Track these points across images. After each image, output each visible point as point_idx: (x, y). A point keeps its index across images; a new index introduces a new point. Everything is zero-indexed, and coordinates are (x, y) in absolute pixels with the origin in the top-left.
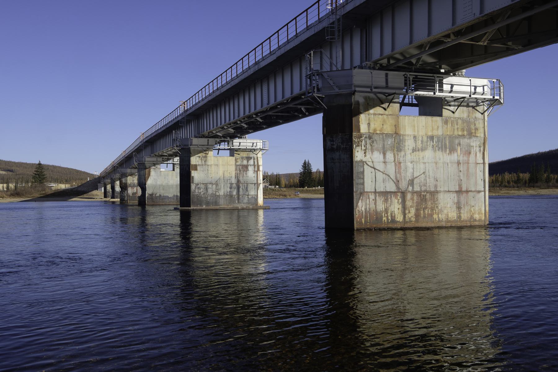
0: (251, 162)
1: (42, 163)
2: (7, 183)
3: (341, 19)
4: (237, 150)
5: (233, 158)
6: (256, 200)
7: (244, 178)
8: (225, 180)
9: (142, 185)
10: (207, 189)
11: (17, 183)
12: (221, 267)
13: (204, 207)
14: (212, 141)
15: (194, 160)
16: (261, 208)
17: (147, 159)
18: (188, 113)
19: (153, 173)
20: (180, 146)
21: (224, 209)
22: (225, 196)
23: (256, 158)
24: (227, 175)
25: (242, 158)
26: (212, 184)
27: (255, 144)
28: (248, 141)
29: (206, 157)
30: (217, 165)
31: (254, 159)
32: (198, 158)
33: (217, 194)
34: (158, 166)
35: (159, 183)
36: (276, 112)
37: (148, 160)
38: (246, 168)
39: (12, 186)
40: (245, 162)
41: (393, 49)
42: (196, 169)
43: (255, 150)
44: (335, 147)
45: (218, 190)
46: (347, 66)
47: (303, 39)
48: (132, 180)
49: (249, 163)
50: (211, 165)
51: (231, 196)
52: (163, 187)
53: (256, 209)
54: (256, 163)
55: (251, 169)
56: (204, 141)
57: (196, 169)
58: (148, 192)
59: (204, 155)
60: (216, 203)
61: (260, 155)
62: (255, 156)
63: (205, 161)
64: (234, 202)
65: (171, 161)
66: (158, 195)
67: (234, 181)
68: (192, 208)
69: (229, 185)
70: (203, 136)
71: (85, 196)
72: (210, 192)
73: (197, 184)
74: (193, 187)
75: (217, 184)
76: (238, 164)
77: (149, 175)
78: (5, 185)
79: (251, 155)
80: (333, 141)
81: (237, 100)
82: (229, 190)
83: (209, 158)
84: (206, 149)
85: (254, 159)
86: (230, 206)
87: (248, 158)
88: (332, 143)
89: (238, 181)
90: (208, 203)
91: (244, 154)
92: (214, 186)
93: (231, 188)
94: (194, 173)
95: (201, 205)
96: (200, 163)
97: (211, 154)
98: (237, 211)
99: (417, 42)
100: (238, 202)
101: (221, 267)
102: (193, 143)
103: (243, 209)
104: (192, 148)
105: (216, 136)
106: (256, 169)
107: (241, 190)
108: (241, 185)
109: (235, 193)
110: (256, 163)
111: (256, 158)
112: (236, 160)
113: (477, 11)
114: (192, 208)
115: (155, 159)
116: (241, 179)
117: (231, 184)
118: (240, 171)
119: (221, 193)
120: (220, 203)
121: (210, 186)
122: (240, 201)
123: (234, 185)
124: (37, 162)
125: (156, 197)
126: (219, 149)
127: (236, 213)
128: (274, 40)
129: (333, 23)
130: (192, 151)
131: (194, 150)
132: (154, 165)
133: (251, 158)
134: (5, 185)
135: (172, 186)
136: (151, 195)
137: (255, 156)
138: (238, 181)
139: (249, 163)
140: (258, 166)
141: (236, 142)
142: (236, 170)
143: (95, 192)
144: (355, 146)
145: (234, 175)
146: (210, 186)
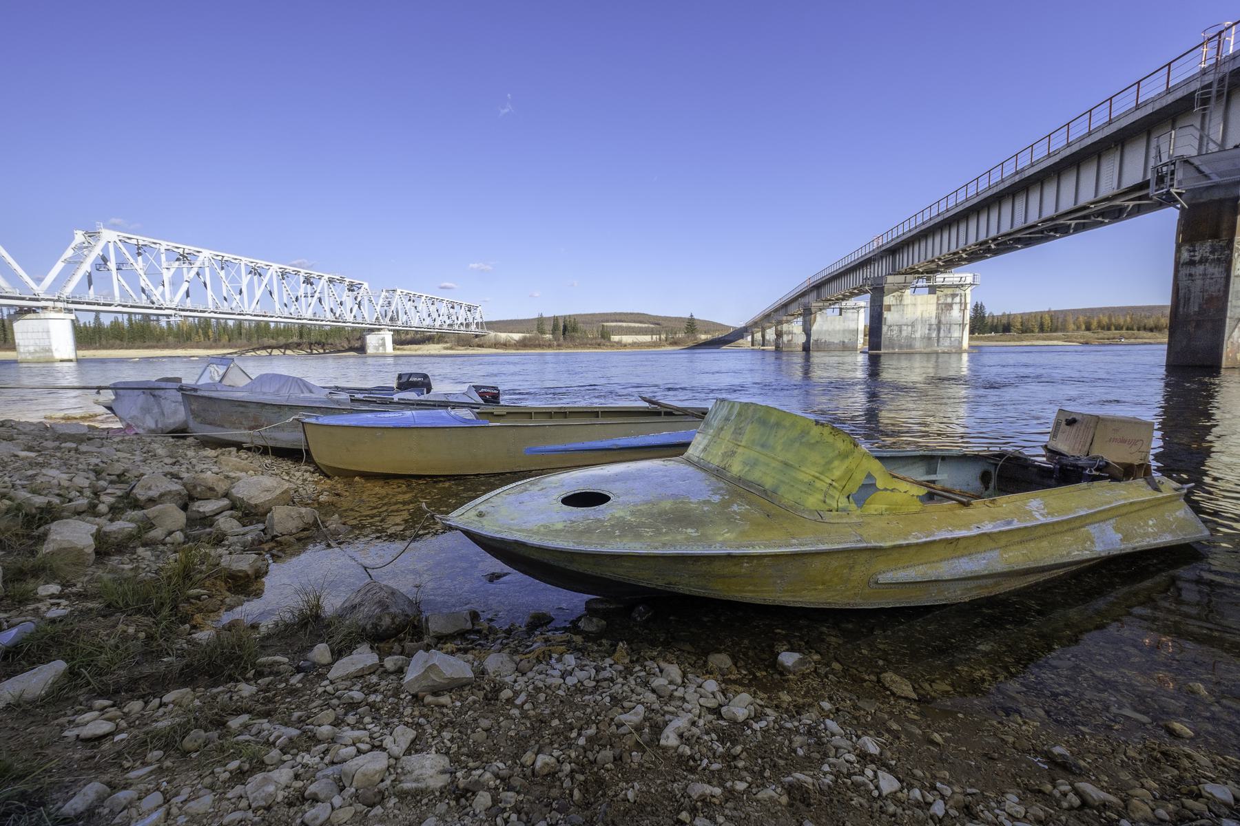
0: (957, 299)
1: (695, 317)
2: (660, 335)
3: (1227, 77)
4: (940, 287)
5: (935, 296)
6: (961, 342)
7: (947, 318)
8: (923, 321)
9: (807, 331)
10: (901, 331)
11: (667, 334)
12: (961, 441)
13: (897, 350)
14: (909, 277)
15: (888, 300)
16: (965, 351)
17: (813, 305)
18: (884, 248)
19: (819, 318)
20: (872, 285)
21: (921, 353)
22: (922, 338)
23: (963, 295)
24: (926, 315)
25: (946, 295)
26: (908, 325)
27: (963, 279)
28: (956, 275)
29: (902, 296)
30: (915, 305)
31: (961, 296)
32: (892, 299)
33: (913, 336)
34: (824, 311)
35: (825, 328)
36: (1030, 233)
37: (815, 305)
38: (949, 306)
39: (663, 337)
40: (949, 300)
41: (941, 253)
42: (890, 310)
43: (962, 285)
44: (1197, 258)
45: (914, 332)
46: (884, 274)
47: (1170, 102)
48: (796, 327)
49: (954, 301)
50: (907, 305)
51: (929, 339)
52: (829, 333)
53: (960, 352)
54: (963, 301)
55: (956, 308)
56: (900, 279)
57: (890, 310)
58: (813, 338)
59: (899, 294)
60: (910, 346)
61: (968, 292)
62: (963, 292)
63: (901, 301)
64: (932, 346)
65: (837, 306)
66: (823, 341)
67: (934, 321)
68: (882, 351)
69: (927, 326)
70: (899, 273)
71: (732, 344)
72: (904, 334)
73: (890, 326)
74: (885, 329)
75: (913, 325)
76: (940, 302)
77: (815, 320)
78: (658, 337)
79: (958, 291)
80: (1194, 251)
81: (939, 237)
82: (927, 331)
83: (905, 297)
84: (901, 288)
85: (961, 296)
86: (928, 350)
87: (954, 296)
88: (1192, 254)
89: (939, 322)
90: (901, 347)
91: (949, 291)
92: (910, 327)
93: (929, 330)
94: (886, 314)
95: (893, 348)
96: (894, 303)
97: (908, 292)
98: (935, 355)
99: (952, 251)
100: (938, 345)
101: (961, 441)
102: (888, 281)
103: (944, 353)
104: (886, 286)
105: (918, 272)
106: (963, 308)
107: (942, 331)
108: (942, 326)
109: (934, 335)
110: (963, 301)
111: (963, 295)
112: (938, 297)
113: (1115, 184)
114: (882, 351)
115: (821, 304)
116: (943, 319)
117: (930, 325)
118: (942, 310)
119: (918, 335)
120: (916, 347)
121: (905, 328)
122: (940, 344)
123: (934, 327)
124: (687, 316)
125: (821, 343)
126: (916, 287)
127: (933, 358)
128: (900, 228)
129: (1210, 85)
130: (885, 290)
131: (888, 289)
132: (821, 310)
133: (957, 295)
134: (658, 337)
135: (839, 331)
136: (817, 341)
137: (963, 292)
138: (939, 322)
139: (954, 301)
140: (966, 304)
141: (939, 278)
142: (937, 309)
143: (741, 341)
144: (1236, 255)
145: (934, 315)
146: (905, 328)
